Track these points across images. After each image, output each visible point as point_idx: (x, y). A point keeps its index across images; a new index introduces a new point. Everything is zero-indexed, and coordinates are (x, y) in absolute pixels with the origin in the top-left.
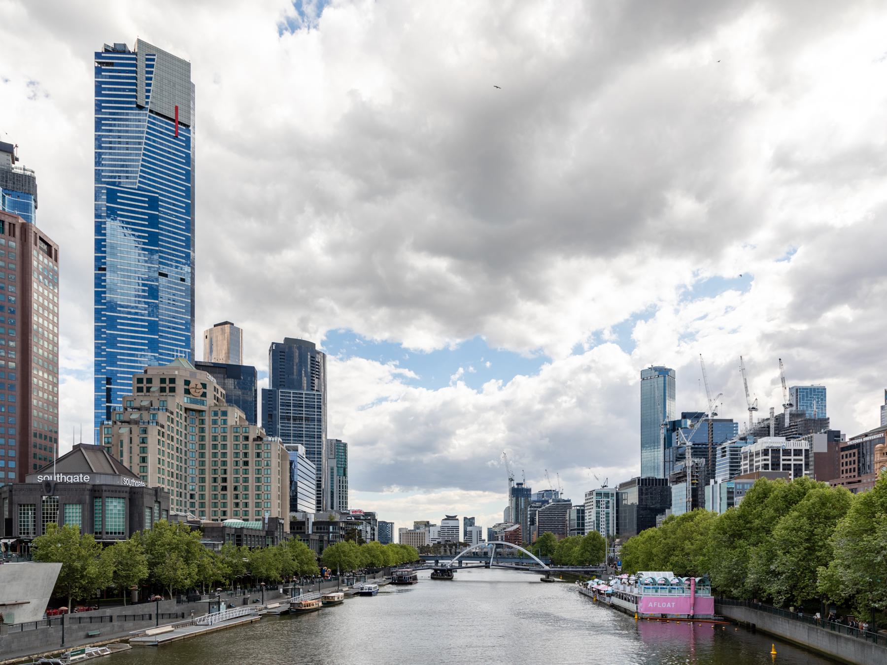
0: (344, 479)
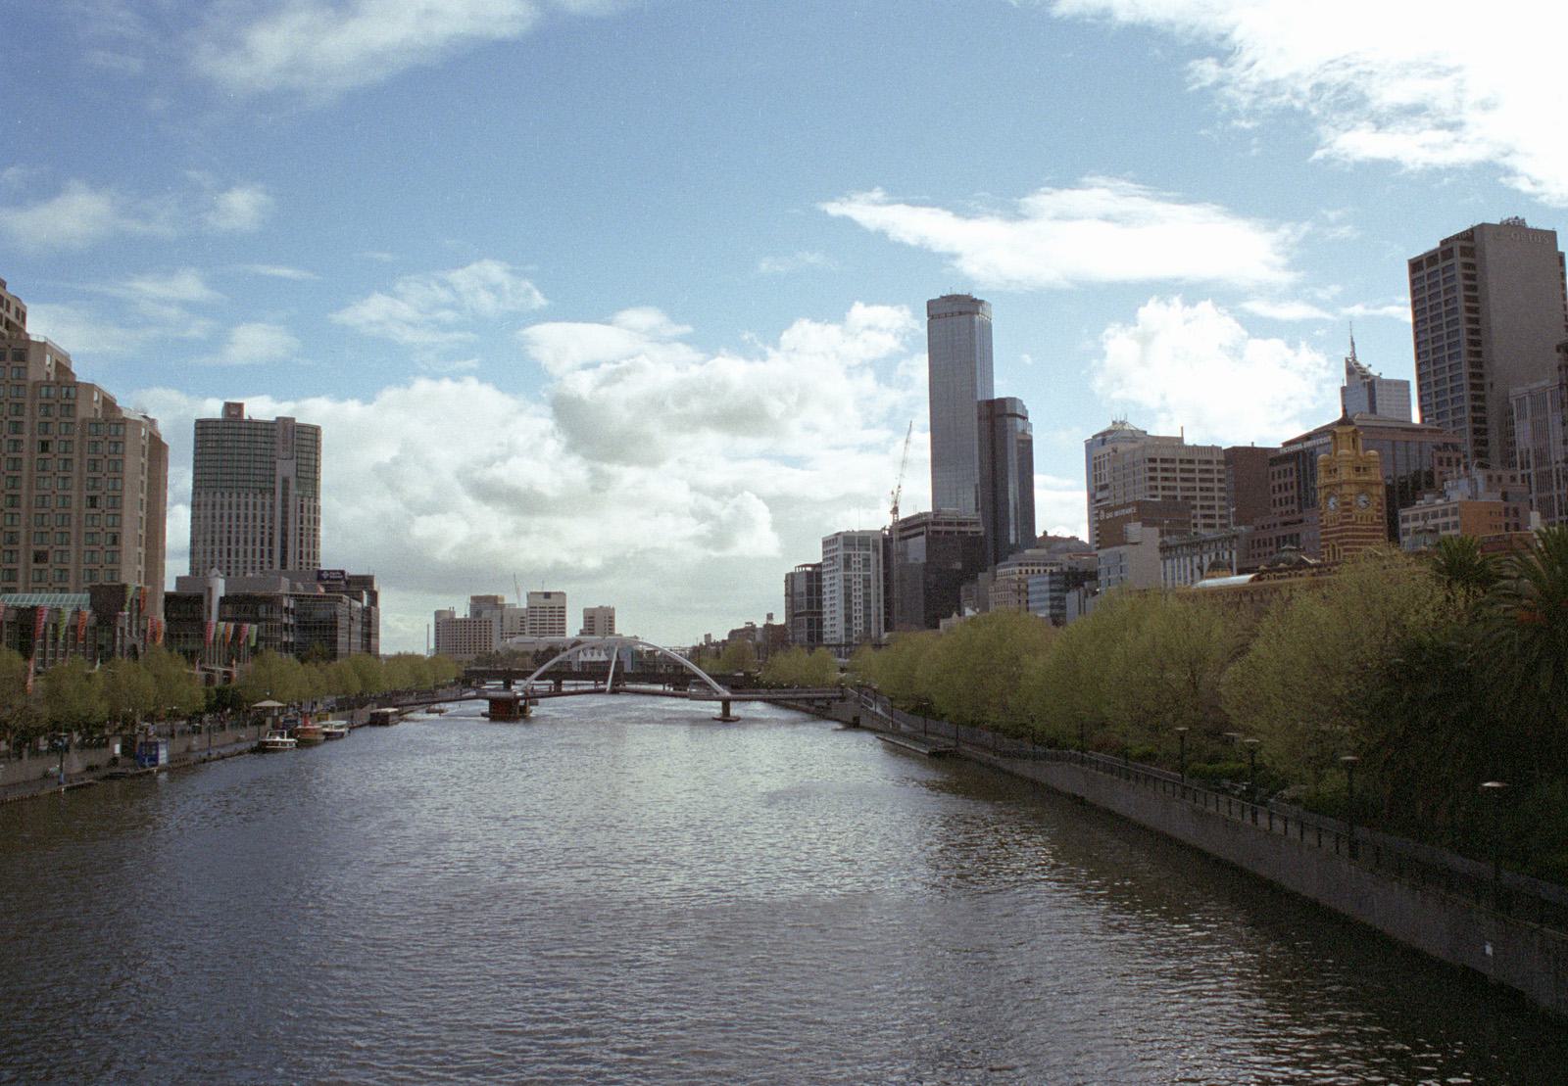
0: (312, 504)
